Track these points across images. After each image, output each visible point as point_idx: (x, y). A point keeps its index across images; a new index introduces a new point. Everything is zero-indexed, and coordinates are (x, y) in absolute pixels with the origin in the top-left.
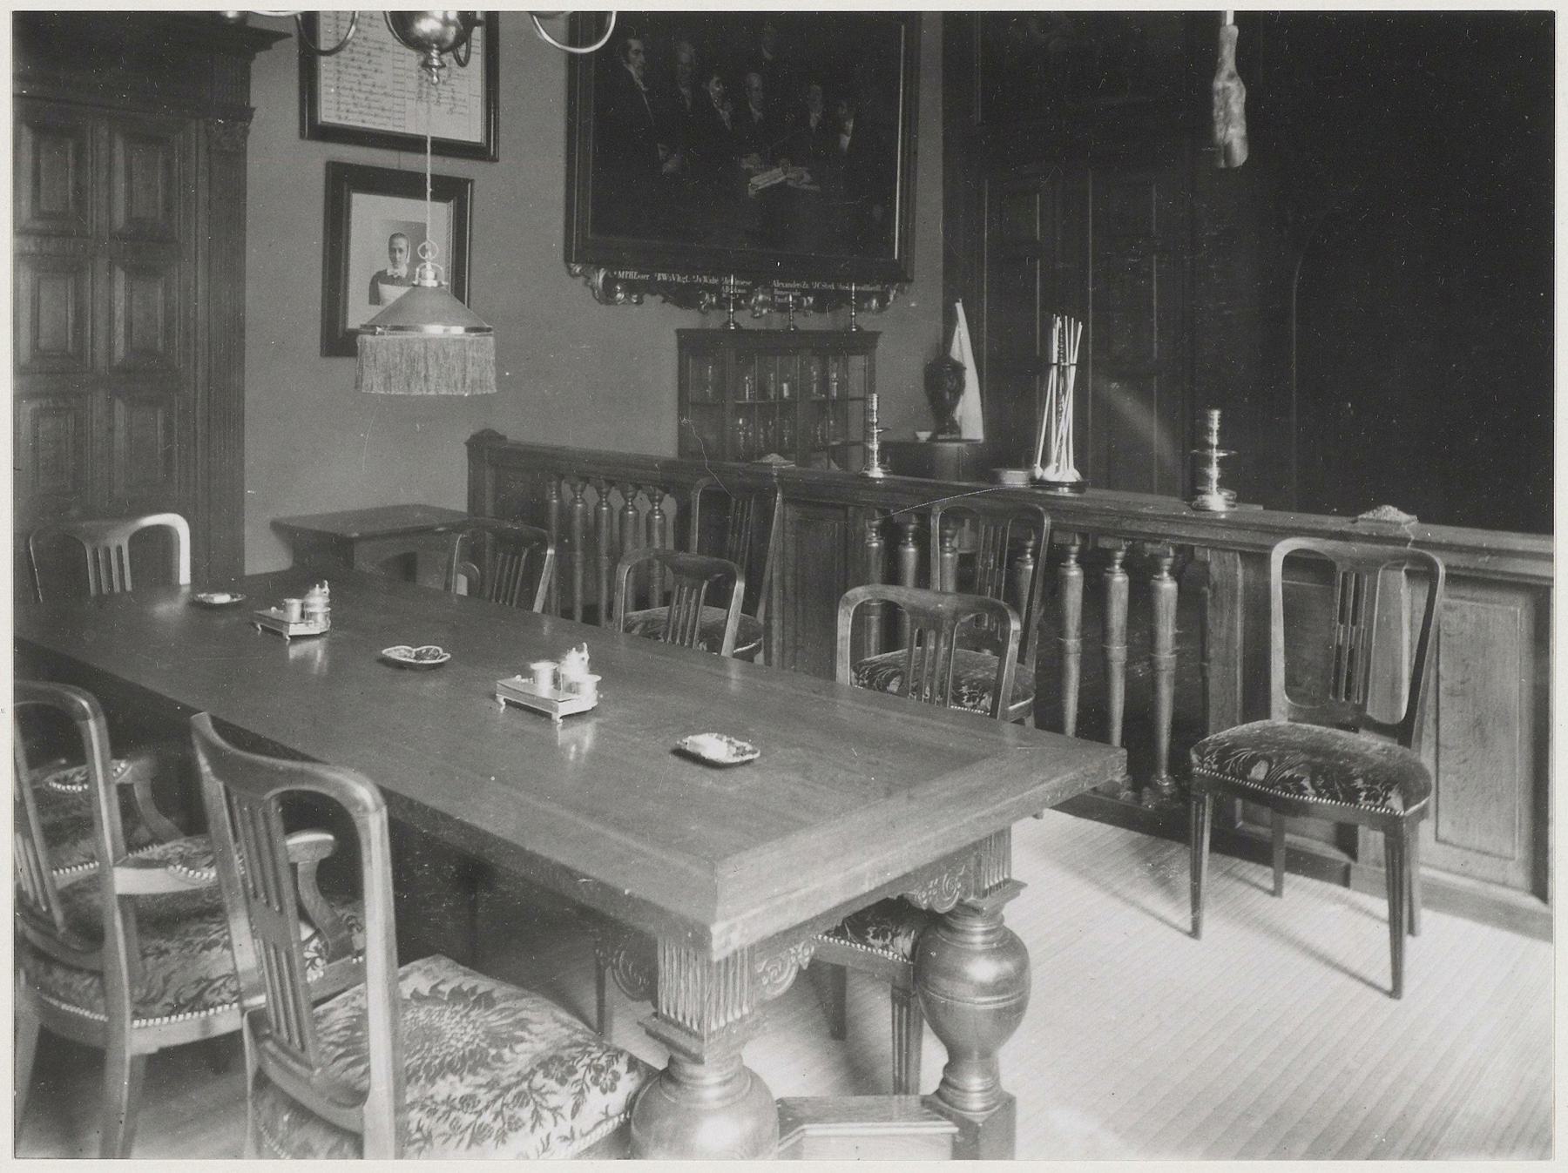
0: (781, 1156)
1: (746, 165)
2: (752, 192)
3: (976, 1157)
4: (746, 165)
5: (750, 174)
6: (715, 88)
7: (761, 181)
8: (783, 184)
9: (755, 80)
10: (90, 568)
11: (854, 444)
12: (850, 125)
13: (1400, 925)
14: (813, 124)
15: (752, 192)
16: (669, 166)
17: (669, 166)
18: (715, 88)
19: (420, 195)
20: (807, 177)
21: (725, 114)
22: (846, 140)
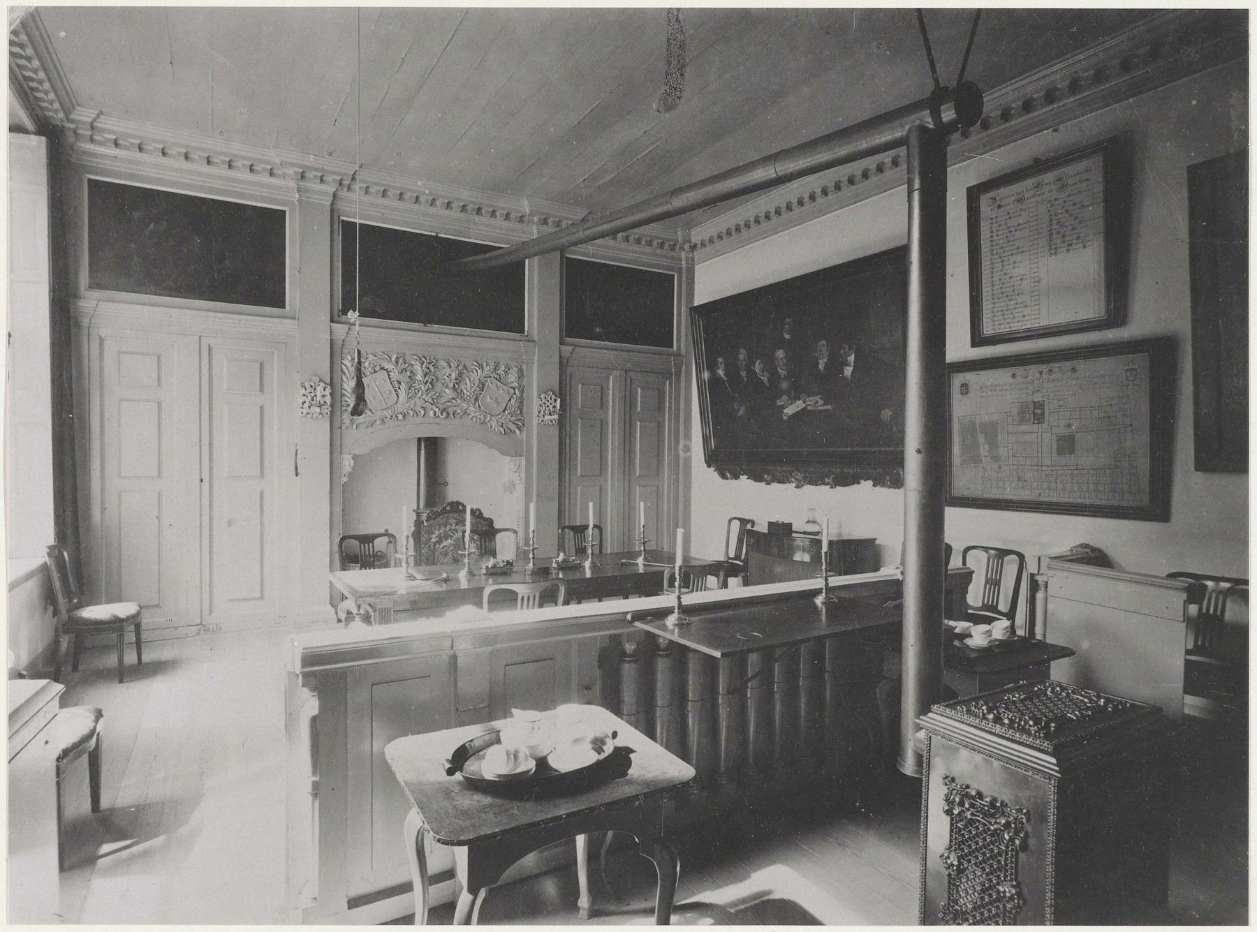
0: (12, 114)
1: (779, 403)
2: (785, 418)
3: (78, 922)
4: (779, 403)
5: (783, 407)
6: (757, 367)
7: (790, 410)
8: (804, 409)
9: (780, 354)
10: (535, 474)
11: (827, 584)
12: (852, 358)
13: (680, 603)
14: (821, 367)
15: (785, 418)
16: (740, 413)
17: (740, 413)
18: (757, 367)
19: (507, 317)
20: (821, 402)
21: (765, 379)
22: (848, 371)
